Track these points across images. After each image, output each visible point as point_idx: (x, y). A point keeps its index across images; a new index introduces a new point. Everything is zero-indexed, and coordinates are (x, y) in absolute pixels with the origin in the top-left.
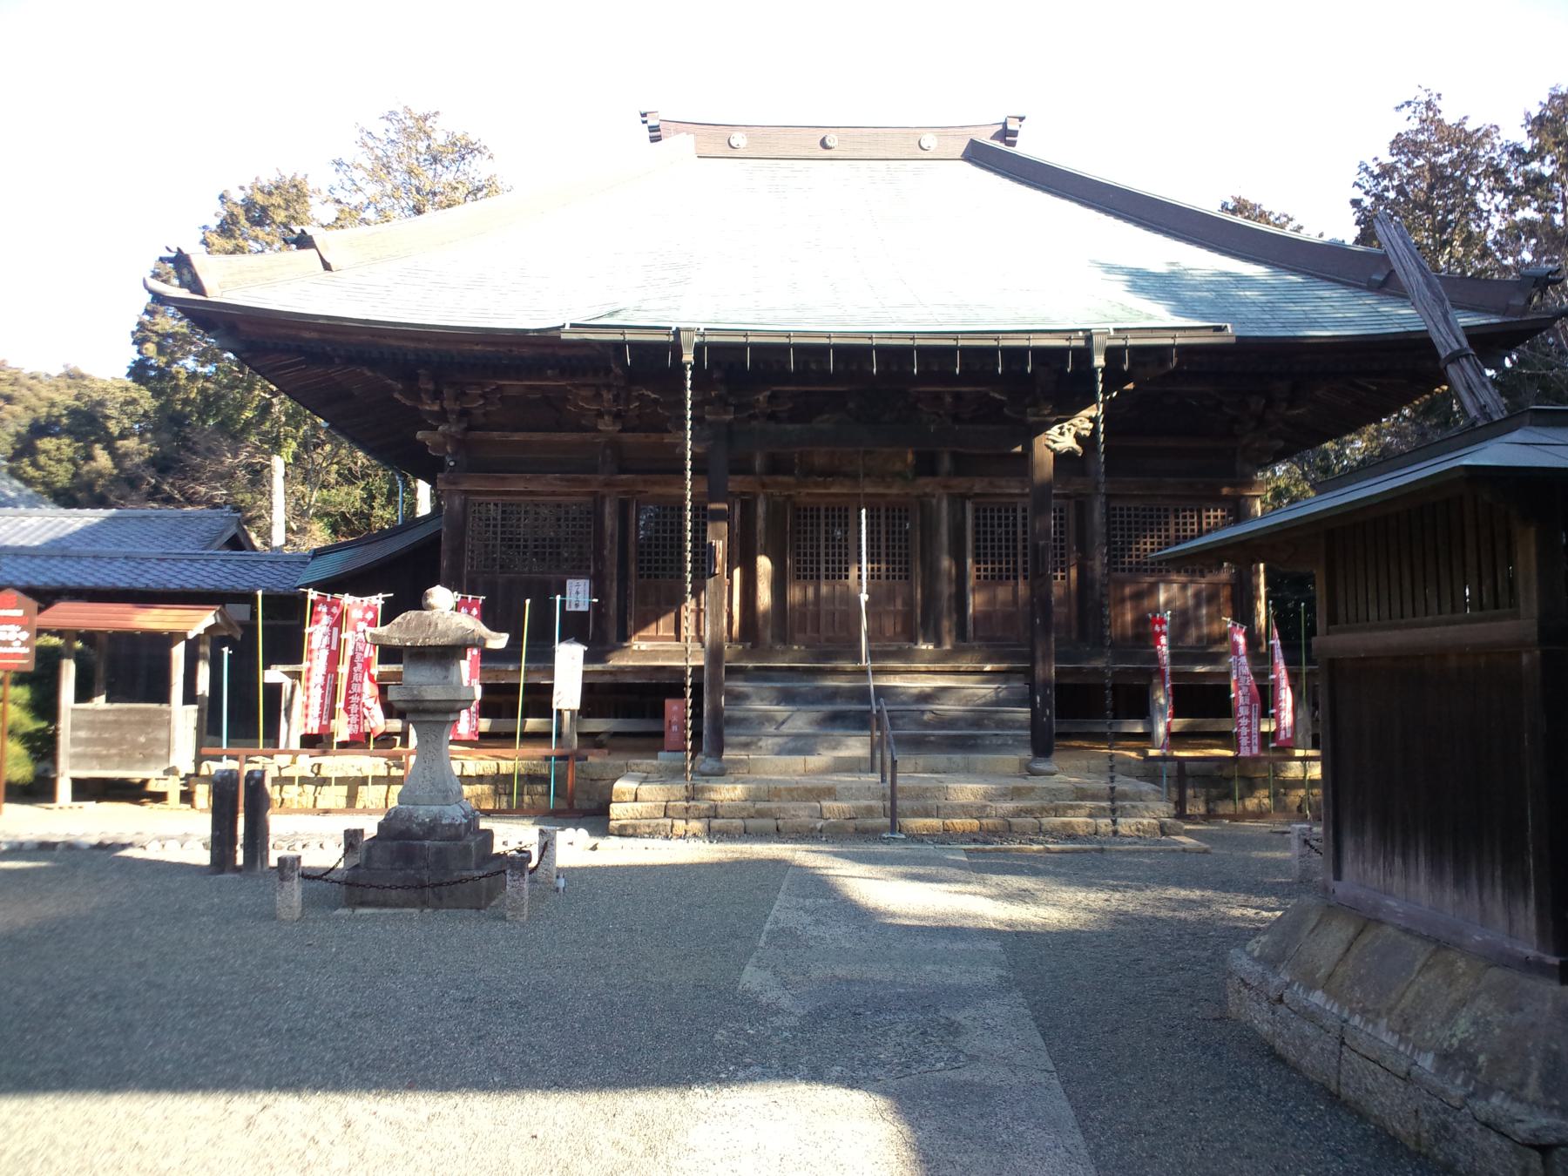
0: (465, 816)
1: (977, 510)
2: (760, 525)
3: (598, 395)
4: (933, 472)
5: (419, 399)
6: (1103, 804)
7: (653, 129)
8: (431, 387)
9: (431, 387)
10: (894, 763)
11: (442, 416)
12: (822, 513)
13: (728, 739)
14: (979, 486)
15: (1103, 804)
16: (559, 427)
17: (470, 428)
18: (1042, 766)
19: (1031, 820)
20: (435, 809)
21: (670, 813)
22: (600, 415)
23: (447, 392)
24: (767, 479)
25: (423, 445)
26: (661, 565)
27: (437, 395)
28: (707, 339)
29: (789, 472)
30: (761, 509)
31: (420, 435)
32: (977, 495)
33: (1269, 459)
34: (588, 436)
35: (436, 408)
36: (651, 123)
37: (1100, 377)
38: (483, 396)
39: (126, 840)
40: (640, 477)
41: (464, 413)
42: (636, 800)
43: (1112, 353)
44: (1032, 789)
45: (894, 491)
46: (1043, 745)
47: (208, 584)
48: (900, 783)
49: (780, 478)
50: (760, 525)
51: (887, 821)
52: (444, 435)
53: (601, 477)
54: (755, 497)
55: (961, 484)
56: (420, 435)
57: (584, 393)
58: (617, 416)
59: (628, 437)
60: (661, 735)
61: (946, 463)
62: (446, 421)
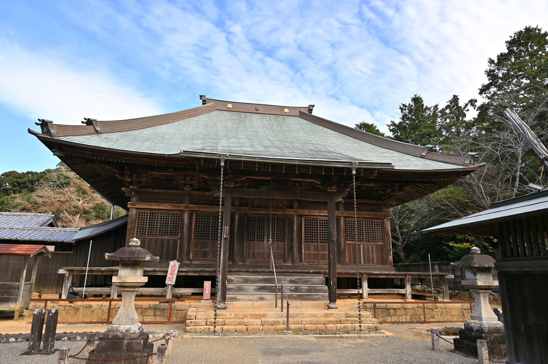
0: (139, 329)
1: (305, 220)
2: (236, 223)
3: (185, 179)
4: (292, 208)
5: (124, 177)
6: (356, 319)
7: (203, 101)
8: (129, 173)
9: (129, 173)
10: (288, 305)
11: (132, 183)
12: (256, 220)
13: (227, 296)
14: (306, 212)
15: (356, 319)
16: (171, 189)
17: (140, 187)
18: (332, 305)
19: (333, 325)
20: (128, 327)
21: (208, 323)
22: (185, 185)
23: (135, 175)
24: (239, 208)
25: (124, 192)
26: (202, 235)
27: (130, 176)
28: (229, 158)
29: (247, 206)
30: (237, 218)
31: (123, 189)
32: (306, 215)
33: (141, 243)
34: (180, 191)
35: (129, 180)
36: (203, 99)
37: (354, 177)
38: (146, 177)
39: (25, 356)
40: (197, 206)
41: (139, 182)
42: (433, 349)
43: (358, 170)
44: (332, 314)
45: (280, 213)
46: (332, 299)
47: (41, 238)
48: (290, 312)
49: (244, 208)
50: (236, 223)
51: (285, 326)
52: (132, 189)
53: (184, 205)
54: (235, 213)
55: (301, 212)
56: (123, 189)
57: (180, 177)
58: (191, 185)
59: (194, 192)
60: (202, 294)
61: (296, 204)
62: (132, 185)
